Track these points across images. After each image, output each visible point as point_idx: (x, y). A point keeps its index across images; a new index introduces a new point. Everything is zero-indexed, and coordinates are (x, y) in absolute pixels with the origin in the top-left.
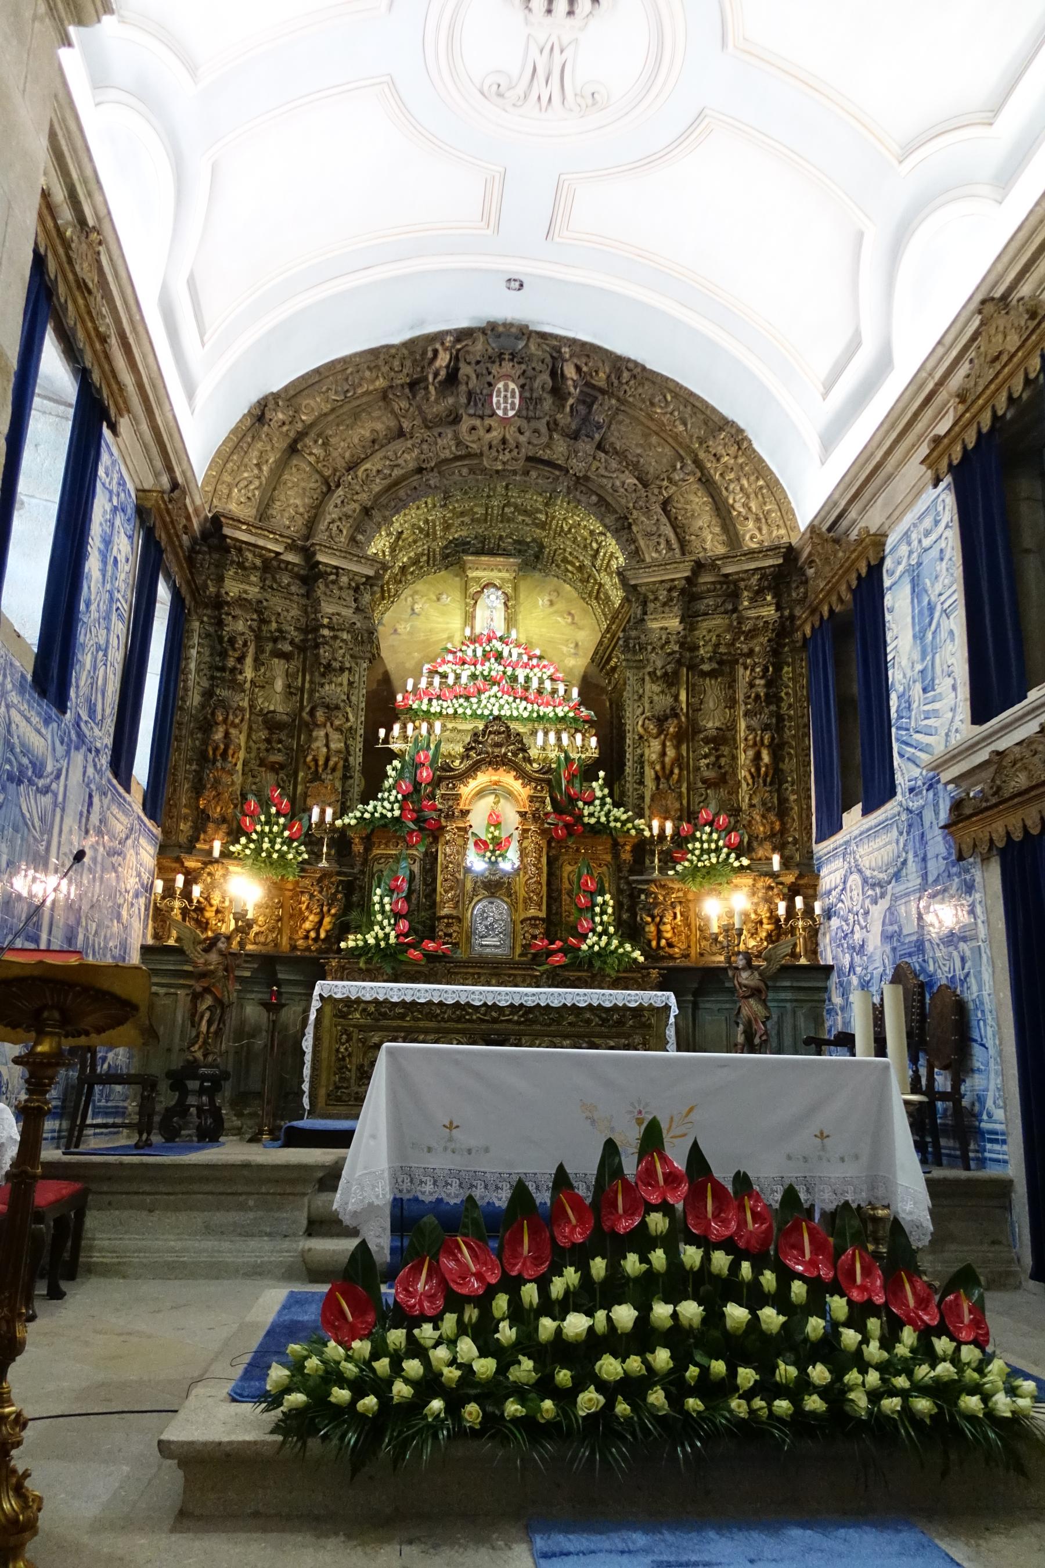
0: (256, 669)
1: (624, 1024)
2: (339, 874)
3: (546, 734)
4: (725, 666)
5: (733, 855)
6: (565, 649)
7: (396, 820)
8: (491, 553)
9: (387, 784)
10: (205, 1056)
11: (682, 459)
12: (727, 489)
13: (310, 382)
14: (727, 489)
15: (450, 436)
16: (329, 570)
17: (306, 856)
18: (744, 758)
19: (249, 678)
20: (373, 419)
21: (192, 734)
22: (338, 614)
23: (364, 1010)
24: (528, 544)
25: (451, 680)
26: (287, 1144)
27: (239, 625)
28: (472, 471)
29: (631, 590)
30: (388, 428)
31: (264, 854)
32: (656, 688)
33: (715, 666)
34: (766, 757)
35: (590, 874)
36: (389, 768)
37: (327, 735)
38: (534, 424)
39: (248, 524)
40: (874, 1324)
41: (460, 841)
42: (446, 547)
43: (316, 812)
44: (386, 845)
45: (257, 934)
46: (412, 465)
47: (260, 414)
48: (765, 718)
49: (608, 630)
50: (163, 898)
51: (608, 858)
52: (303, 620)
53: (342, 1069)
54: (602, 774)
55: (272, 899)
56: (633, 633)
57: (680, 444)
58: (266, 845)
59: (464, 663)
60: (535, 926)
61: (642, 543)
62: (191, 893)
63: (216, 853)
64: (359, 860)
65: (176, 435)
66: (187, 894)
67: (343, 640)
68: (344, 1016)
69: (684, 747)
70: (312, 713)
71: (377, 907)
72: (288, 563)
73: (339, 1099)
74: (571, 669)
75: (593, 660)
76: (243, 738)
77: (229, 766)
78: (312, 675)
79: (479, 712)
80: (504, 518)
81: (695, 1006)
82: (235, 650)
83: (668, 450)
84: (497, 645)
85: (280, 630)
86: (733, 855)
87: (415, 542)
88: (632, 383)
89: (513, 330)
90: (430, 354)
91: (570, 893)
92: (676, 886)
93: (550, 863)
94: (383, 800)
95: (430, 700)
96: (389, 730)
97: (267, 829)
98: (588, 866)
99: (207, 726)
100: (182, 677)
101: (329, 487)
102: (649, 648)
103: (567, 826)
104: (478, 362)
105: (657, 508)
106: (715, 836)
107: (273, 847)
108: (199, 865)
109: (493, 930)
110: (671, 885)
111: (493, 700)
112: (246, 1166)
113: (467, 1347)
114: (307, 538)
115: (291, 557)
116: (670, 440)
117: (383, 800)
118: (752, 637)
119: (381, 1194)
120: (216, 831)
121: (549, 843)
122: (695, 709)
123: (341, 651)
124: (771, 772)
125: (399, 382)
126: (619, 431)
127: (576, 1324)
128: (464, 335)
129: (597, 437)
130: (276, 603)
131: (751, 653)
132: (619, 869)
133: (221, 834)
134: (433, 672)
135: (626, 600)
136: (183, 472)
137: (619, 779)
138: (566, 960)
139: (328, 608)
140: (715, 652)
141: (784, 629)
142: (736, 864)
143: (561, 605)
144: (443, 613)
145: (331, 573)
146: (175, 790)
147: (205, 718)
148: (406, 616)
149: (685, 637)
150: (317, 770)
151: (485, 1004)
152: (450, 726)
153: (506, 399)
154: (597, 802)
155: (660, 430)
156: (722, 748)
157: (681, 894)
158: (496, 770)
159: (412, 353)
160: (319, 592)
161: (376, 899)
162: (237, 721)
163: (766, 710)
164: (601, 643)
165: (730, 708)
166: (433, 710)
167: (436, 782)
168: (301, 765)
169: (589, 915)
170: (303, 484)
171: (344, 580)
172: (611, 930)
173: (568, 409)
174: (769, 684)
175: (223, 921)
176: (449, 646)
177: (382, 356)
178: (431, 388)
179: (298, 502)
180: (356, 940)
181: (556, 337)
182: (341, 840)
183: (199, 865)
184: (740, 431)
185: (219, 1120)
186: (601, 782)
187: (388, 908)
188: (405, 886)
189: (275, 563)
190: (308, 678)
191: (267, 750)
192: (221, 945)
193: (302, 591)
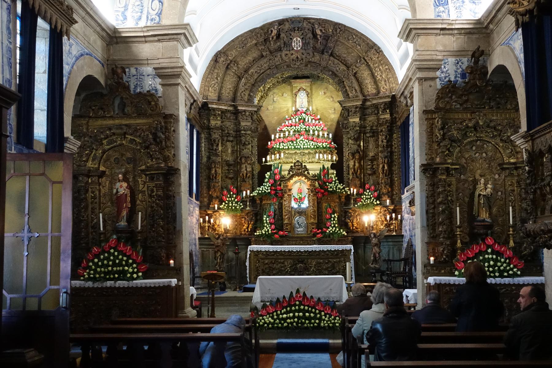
0: (222, 146)
4: (375, 134)
6: (330, 111)
25: (287, 133)
26: (244, 291)
33: (371, 134)
38: (307, 51)
40: (328, 316)
43: (244, 192)
46: (267, 68)
47: (216, 59)
48: (386, 154)
51: (338, 200)
52: (235, 128)
58: (230, 205)
63: (216, 208)
64: (259, 206)
66: (209, 222)
67: (249, 134)
68: (257, 255)
70: (241, 159)
76: (220, 170)
90: (270, 32)
93: (318, 203)
94: (265, 186)
95: (280, 143)
99: (210, 169)
105: (353, 78)
111: (301, 142)
112: (235, 297)
113: (270, 319)
119: (259, 300)
122: (366, 147)
127: (285, 316)
128: (281, 22)
129: (330, 52)
131: (382, 131)
133: (217, 202)
138: (322, 236)
139: (243, 124)
142: (375, 203)
143: (328, 94)
144: (284, 101)
148: (271, 103)
153: (297, 43)
161: (264, 219)
171: (247, 113)
172: (336, 225)
174: (387, 142)
178: (272, 43)
182: (253, 200)
184: (379, 48)
192: (221, 238)
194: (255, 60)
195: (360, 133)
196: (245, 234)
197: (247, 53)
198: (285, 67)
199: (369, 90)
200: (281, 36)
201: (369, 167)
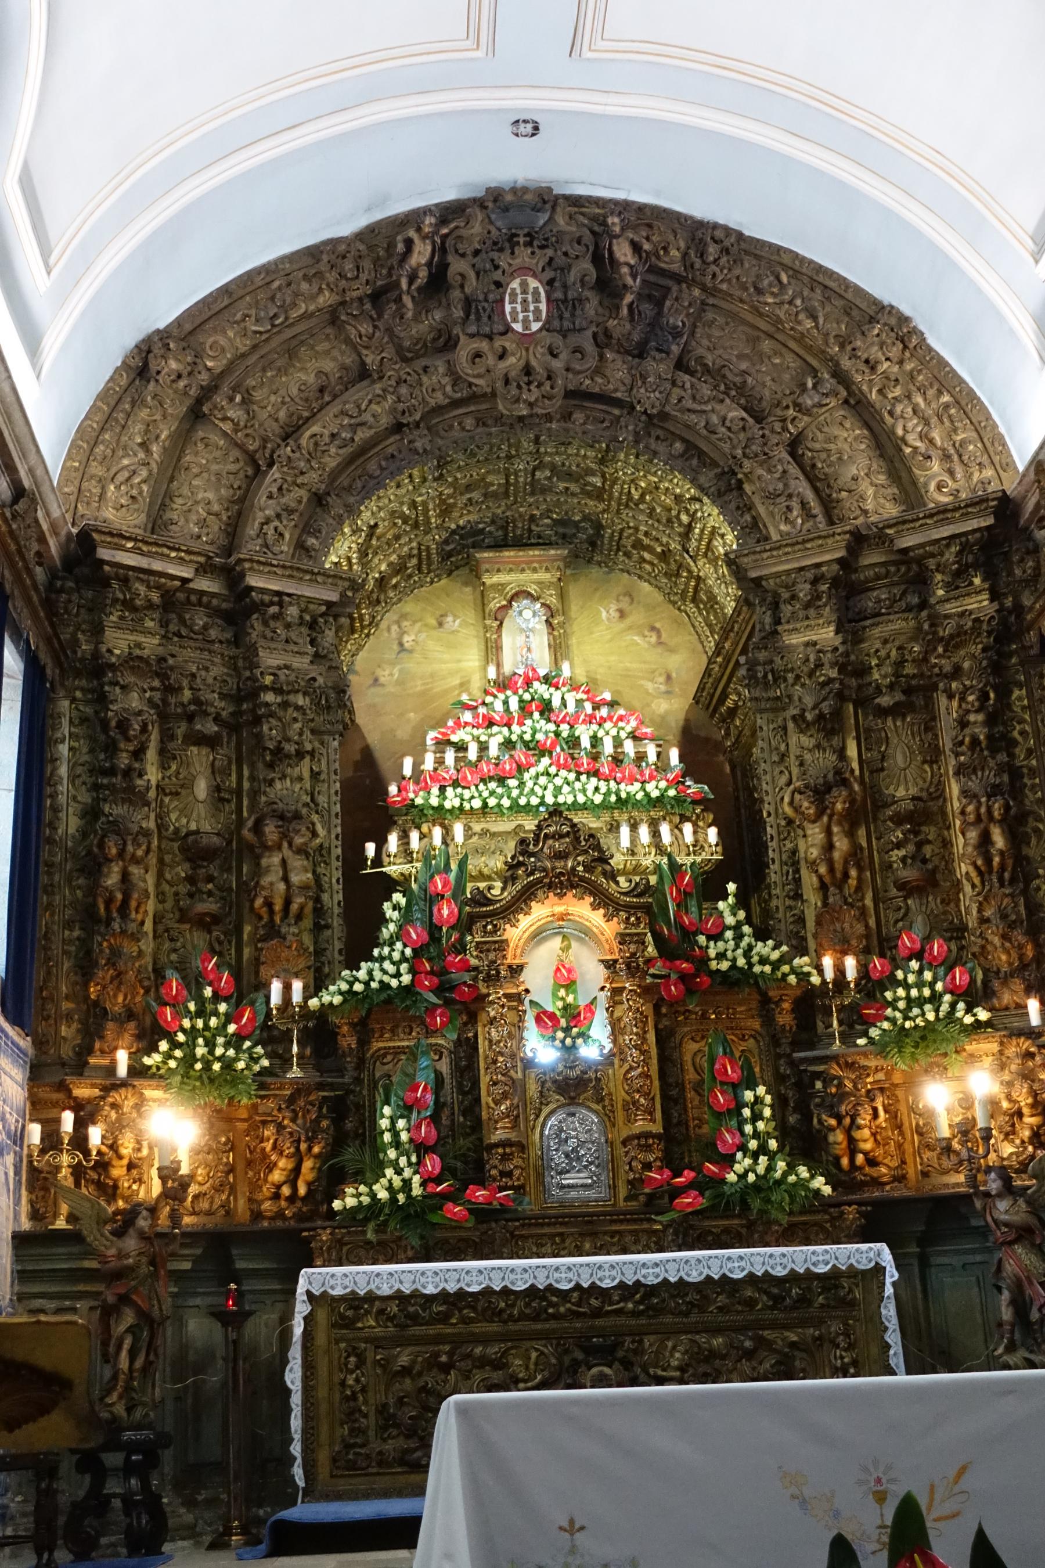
0: (164, 767)
1: (810, 1303)
2: (321, 1086)
3: (634, 827)
4: (916, 696)
5: (961, 1005)
6: (650, 686)
7: (405, 991)
8: (520, 544)
9: (385, 934)
10: (129, 1410)
11: (814, 373)
12: (891, 413)
13: (216, 308)
14: (891, 413)
15: (441, 370)
16: (267, 598)
17: (266, 1063)
18: (963, 843)
19: (153, 782)
20: (317, 356)
21: (69, 880)
22: (287, 667)
23: (381, 1312)
24: (576, 524)
25: (472, 754)
27: (133, 700)
28: (481, 422)
29: (752, 587)
30: (344, 367)
31: (198, 1066)
32: (807, 741)
33: (899, 697)
34: (999, 840)
35: (729, 1054)
36: (387, 906)
37: (284, 862)
38: (574, 340)
39: (135, 540)
41: (511, 1017)
42: (446, 542)
43: (276, 988)
44: (392, 1031)
45: (196, 1197)
46: (385, 421)
47: (142, 365)
49: (718, 652)
50: (43, 1151)
51: (756, 1024)
52: (232, 682)
53: (352, 1414)
54: (731, 887)
55: (215, 1137)
56: (762, 656)
57: (809, 349)
58: (200, 1051)
59: (491, 723)
60: (648, 1148)
61: (762, 510)
62: (86, 1139)
63: (122, 1071)
65: (17, 416)
66: (80, 1141)
67: (298, 708)
68: (348, 1324)
69: (862, 832)
70: (258, 828)
71: (387, 1137)
72: (202, 593)
73: (352, 1466)
74: (663, 717)
75: (697, 699)
76: (151, 879)
77: (132, 927)
78: (252, 766)
79: (523, 801)
80: (536, 488)
81: (924, 1262)
82: (128, 739)
83: (790, 358)
84: (541, 689)
85: (196, 701)
86: (961, 1005)
87: (397, 538)
88: (724, 260)
89: (528, 197)
90: (400, 247)
91: (698, 1087)
92: (872, 1063)
94: (381, 959)
95: (442, 789)
96: (381, 843)
97: (200, 1023)
98: (725, 1043)
99: (92, 866)
100: (49, 790)
101: (256, 467)
102: (790, 676)
103: (683, 978)
104: (477, 253)
106: (928, 976)
107: (211, 1052)
108: (97, 1092)
109: (579, 1159)
110: (863, 1062)
111: (543, 780)
114: (228, 550)
115: (206, 584)
116: (792, 345)
117: (381, 959)
118: (957, 647)
120: (119, 1035)
121: (657, 1008)
122: (874, 768)
123: (297, 726)
124: (1010, 862)
125: (355, 294)
126: (709, 337)
128: (451, 212)
129: (675, 349)
130: (188, 657)
132: (775, 1041)
133: (127, 1039)
134: (443, 744)
135: (744, 602)
136: (31, 471)
137: (757, 889)
138: (703, 1202)
139: (270, 659)
140: (897, 675)
141: (1006, 629)
142: (968, 1020)
143: (637, 617)
145: (272, 603)
146: (49, 973)
147: (89, 853)
148: (390, 655)
149: (847, 654)
150: (272, 920)
151: (578, 1287)
152: (477, 828)
153: (525, 304)
154: (729, 934)
155: (776, 330)
156: (924, 829)
157: (881, 1076)
158: (561, 896)
159: (371, 248)
160: (254, 635)
161: (384, 1123)
162: (140, 853)
163: (992, 763)
164: (708, 673)
165: (931, 763)
166: (448, 805)
167: (465, 924)
168: (246, 911)
169: (734, 1123)
170: (215, 467)
171: (293, 611)
172: (773, 1144)
173: (625, 311)
174: (991, 720)
175: (140, 1181)
176: (465, 698)
177: (325, 258)
178: (407, 300)
179: (210, 495)
180: (358, 1195)
181: (597, 202)
182: (319, 1030)
183: (97, 1092)
185: (158, 1514)
186: (731, 900)
187: (404, 1136)
188: (430, 1098)
189: (181, 596)
190: (246, 773)
191: (191, 895)
192: (142, 1223)
193: (228, 635)
194: (324, 392)
195: (841, 697)
196: (280, 1215)
197: (291, 353)
198: (469, 423)
199: (869, 505)
200: (451, 271)
201: (897, 854)
